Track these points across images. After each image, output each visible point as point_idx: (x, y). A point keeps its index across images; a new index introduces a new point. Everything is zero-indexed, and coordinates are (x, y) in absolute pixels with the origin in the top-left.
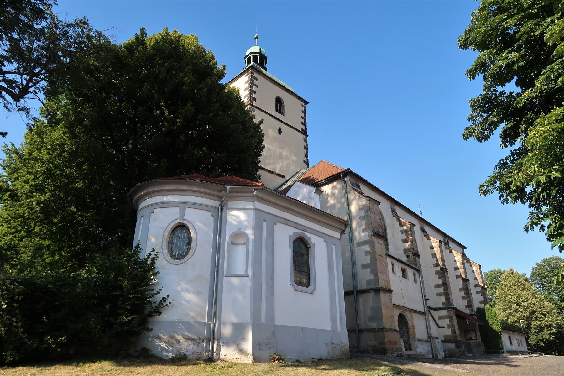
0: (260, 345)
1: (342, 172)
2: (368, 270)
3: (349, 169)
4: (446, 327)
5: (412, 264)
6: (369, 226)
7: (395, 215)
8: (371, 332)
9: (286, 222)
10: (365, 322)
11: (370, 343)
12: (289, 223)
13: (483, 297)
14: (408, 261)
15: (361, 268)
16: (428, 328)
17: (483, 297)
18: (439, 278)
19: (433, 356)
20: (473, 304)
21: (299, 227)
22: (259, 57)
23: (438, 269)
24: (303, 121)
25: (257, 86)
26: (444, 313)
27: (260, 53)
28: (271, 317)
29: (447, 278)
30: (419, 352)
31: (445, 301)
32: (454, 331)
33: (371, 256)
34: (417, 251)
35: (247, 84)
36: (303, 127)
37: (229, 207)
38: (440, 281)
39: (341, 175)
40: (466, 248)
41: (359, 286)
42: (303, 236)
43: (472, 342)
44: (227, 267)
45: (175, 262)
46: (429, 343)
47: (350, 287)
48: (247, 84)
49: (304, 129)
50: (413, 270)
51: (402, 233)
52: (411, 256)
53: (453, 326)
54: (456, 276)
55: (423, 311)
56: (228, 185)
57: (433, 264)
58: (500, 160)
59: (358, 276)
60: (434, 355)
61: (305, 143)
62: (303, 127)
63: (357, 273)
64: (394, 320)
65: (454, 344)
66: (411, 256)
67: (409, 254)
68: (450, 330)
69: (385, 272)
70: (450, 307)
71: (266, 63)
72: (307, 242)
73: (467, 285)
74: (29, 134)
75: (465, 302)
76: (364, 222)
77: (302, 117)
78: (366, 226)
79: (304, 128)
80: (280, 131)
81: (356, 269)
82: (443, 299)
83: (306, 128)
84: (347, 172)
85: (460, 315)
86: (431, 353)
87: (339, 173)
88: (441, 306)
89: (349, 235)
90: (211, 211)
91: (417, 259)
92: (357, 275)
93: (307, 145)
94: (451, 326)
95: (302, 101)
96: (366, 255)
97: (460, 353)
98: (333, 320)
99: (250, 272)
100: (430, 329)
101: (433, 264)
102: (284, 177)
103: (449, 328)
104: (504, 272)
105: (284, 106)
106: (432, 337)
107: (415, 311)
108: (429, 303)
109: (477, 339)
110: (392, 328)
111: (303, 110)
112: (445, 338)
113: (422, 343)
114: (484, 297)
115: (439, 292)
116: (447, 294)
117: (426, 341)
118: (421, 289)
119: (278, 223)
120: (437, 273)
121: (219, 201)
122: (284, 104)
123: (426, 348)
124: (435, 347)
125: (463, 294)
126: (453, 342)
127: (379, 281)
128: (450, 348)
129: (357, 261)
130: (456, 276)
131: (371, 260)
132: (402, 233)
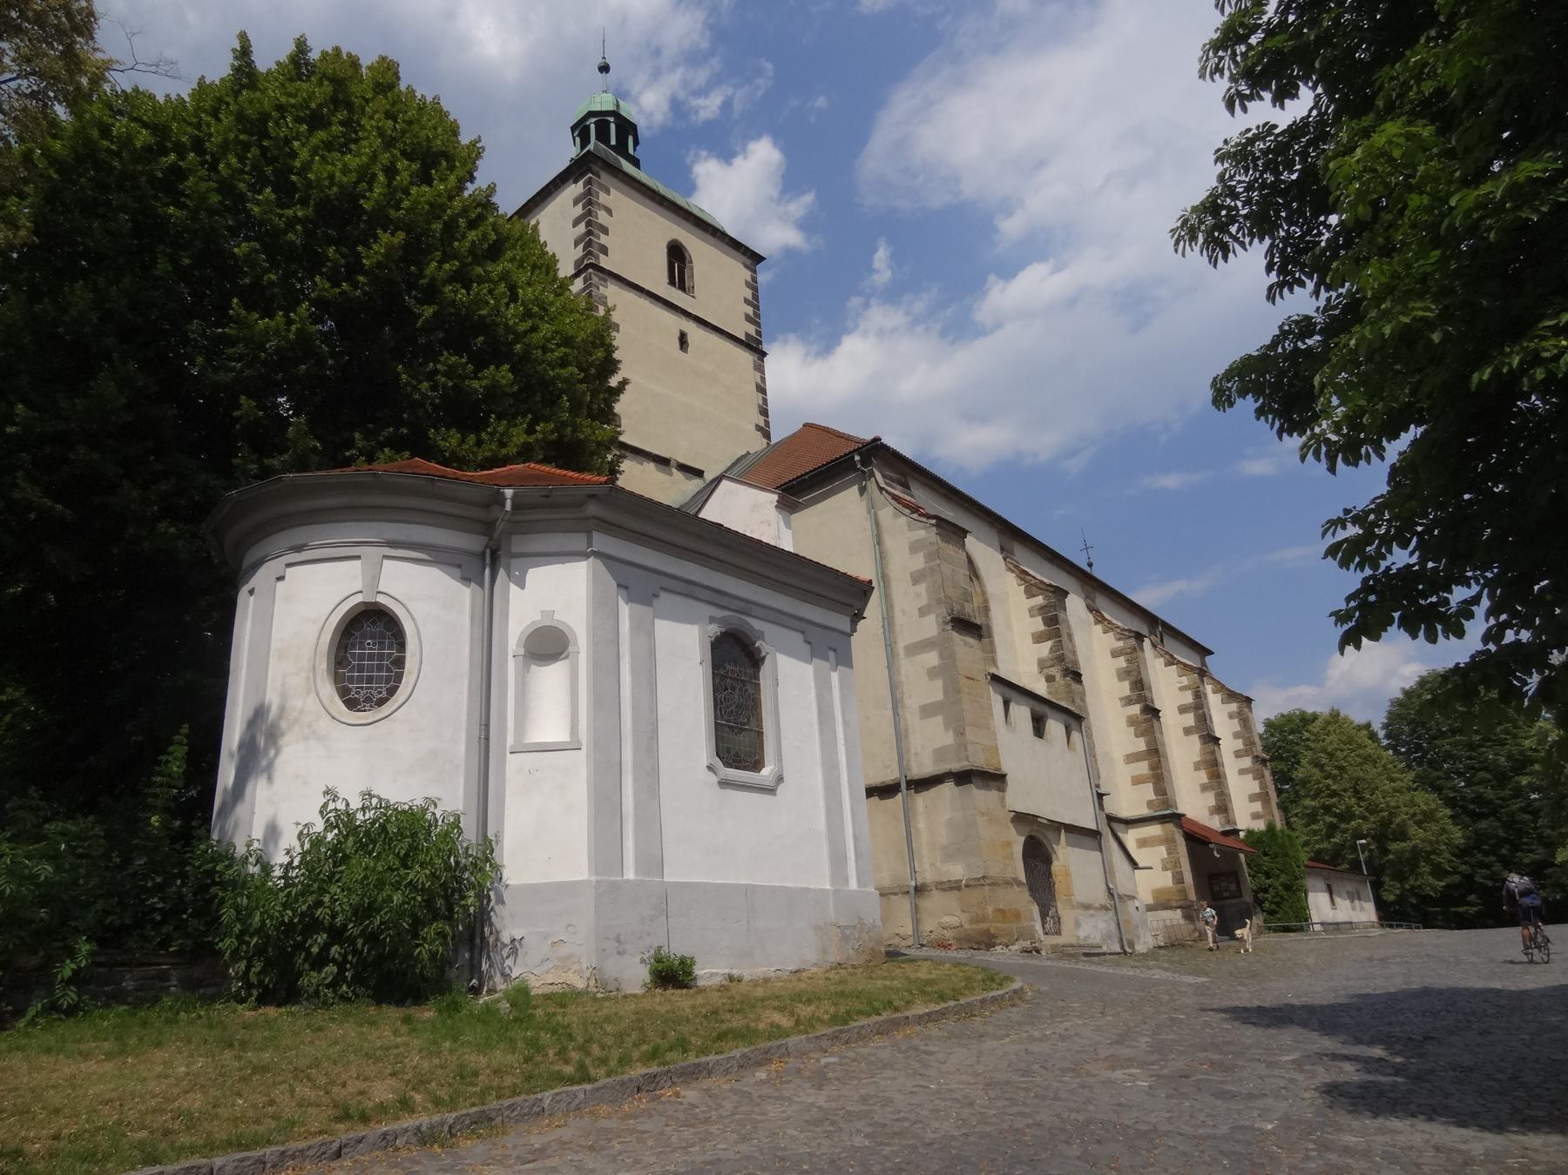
0: (618, 940)
2: (938, 721)
3: (877, 439)
4: (1158, 866)
5: (1062, 699)
7: (1011, 566)
8: (951, 889)
10: (932, 864)
11: (947, 920)
12: (697, 591)
13: (1257, 782)
14: (1049, 693)
16: (1108, 872)
17: (1257, 782)
19: (1122, 948)
20: (1231, 801)
21: (725, 601)
22: (613, 127)
24: (750, 310)
25: (609, 212)
26: (1155, 830)
27: (615, 114)
28: (653, 861)
29: (1158, 735)
30: (1082, 937)
31: (1154, 797)
32: (1179, 879)
33: (944, 681)
34: (1076, 663)
35: (580, 205)
36: (751, 329)
37: (514, 550)
38: (1141, 745)
39: (857, 458)
40: (1210, 653)
41: (913, 765)
42: (739, 627)
44: (506, 719)
45: (358, 718)
46: (1111, 914)
47: (889, 771)
48: (580, 205)
49: (753, 334)
51: (1032, 616)
52: (1058, 677)
53: (1177, 863)
55: (1093, 827)
56: (509, 486)
57: (1121, 699)
60: (1125, 942)
61: (758, 375)
62: (751, 329)
63: (906, 730)
64: (1012, 854)
65: (1179, 911)
66: (1058, 677)
67: (1053, 673)
68: (1169, 874)
69: (985, 725)
70: (1168, 812)
71: (636, 143)
73: (1213, 752)
75: (1210, 799)
76: (922, 588)
77: (746, 301)
79: (753, 333)
80: (683, 340)
81: (906, 720)
82: (1148, 792)
83: (759, 333)
84: (874, 448)
85: (1196, 840)
86: (1116, 940)
87: (850, 453)
88: (1144, 811)
89: (883, 627)
90: (459, 566)
91: (1075, 686)
92: (907, 737)
93: (763, 379)
94: (1171, 864)
95: (744, 254)
96: (931, 680)
98: (837, 860)
100: (1113, 874)
101: (1121, 699)
102: (699, 473)
103: (1165, 869)
104: (1315, 717)
105: (692, 269)
106: (1120, 897)
107: (1072, 829)
108: (1111, 806)
110: (1009, 875)
111: (749, 279)
112: (1155, 898)
113: (1091, 912)
114: (1261, 784)
115: (1137, 773)
116: (1159, 776)
117: (1104, 908)
119: (663, 595)
120: (1132, 721)
121: (484, 535)
122: (691, 262)
123: (1102, 925)
124: (1128, 922)
125: (1203, 777)
126: (1177, 908)
127: (969, 749)
128: (1168, 923)
129: (906, 696)
130: (1184, 728)
131: (946, 693)
132: (1032, 616)
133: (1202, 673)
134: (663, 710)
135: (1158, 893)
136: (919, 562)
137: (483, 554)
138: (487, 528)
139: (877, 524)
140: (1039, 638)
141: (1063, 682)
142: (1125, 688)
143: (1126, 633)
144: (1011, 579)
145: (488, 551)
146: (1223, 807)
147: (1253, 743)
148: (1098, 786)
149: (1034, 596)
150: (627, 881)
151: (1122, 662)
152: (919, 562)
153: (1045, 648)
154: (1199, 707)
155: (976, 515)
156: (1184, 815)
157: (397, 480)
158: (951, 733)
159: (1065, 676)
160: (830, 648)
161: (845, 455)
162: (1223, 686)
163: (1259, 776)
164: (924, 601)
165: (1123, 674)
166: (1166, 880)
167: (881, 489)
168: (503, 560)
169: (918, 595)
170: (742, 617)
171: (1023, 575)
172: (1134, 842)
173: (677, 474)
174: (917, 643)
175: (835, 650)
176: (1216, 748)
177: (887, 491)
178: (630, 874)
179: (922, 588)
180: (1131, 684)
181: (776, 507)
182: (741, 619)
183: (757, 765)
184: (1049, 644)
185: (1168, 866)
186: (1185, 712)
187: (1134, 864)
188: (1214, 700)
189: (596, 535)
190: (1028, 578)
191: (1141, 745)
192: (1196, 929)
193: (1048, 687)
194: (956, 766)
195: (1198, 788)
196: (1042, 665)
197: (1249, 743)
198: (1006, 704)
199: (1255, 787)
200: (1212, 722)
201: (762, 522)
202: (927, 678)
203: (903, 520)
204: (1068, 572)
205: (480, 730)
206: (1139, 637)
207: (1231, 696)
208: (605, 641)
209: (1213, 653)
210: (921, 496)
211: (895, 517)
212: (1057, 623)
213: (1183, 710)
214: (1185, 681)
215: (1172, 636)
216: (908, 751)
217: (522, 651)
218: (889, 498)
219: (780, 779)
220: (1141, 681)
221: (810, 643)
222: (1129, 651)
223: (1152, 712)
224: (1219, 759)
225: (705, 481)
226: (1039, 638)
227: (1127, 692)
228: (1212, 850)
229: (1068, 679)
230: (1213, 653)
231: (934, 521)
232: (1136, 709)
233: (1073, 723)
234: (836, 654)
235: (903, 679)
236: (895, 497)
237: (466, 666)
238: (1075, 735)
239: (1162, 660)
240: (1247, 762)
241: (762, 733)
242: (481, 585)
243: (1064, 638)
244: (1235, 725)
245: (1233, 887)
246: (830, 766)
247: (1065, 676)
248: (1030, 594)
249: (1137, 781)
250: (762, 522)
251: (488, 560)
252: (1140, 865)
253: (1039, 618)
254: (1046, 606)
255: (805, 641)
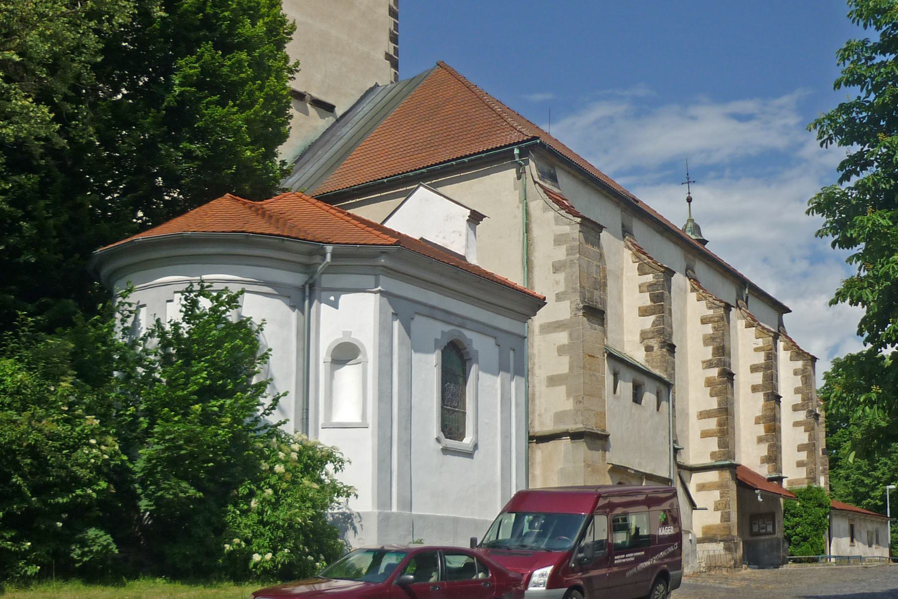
1: (519, 143)
4: (711, 507)
5: (657, 367)
6: (574, 286)
7: (629, 244)
9: (432, 312)
13: (807, 434)
14: (647, 361)
15: (545, 383)
17: (807, 434)
18: (711, 396)
23: (711, 375)
26: (712, 476)
28: (407, 503)
32: (726, 518)
38: (713, 404)
39: (516, 151)
43: (763, 540)
50: (658, 384)
51: (641, 292)
53: (727, 505)
54: (753, 386)
57: (703, 362)
58: (784, 517)
59: (537, 401)
63: (534, 395)
65: (722, 544)
67: (652, 344)
68: (719, 514)
70: (727, 462)
72: (465, 349)
73: (774, 409)
74: (738, 561)
75: (764, 450)
78: (567, 286)
81: (534, 386)
82: (713, 444)
87: (510, 145)
88: (707, 461)
90: (289, 297)
97: (733, 562)
99: (372, 419)
101: (703, 362)
103: (716, 509)
108: (682, 459)
109: (774, 533)
114: (810, 435)
118: (668, 426)
120: (709, 383)
121: (305, 273)
125: (761, 430)
126: (721, 541)
128: (711, 553)
129: (536, 367)
130: (753, 386)
131: (571, 367)
132: (641, 292)
133: (779, 333)
134: (414, 400)
135: (707, 529)
136: (561, 254)
137: (304, 286)
138: (308, 269)
139: (527, 213)
140: (644, 312)
141: (659, 353)
142: (708, 353)
143: (717, 302)
144: (627, 255)
145: (307, 286)
146: (774, 457)
147: (810, 399)
148: (675, 442)
149: (646, 274)
150: (393, 513)
151: (709, 329)
152: (561, 254)
153: (648, 322)
154: (769, 368)
155: (607, 197)
156: (739, 465)
157: (264, 239)
158: (571, 400)
159: (662, 347)
160: (511, 348)
161: (506, 146)
162: (794, 344)
163: (810, 429)
164: (561, 288)
165: (708, 340)
166: (714, 519)
167: (535, 182)
168: (317, 292)
169: (557, 283)
170: (460, 329)
171: (639, 251)
172: (695, 486)
173: (312, 110)
174: (551, 323)
175: (514, 350)
176: (777, 406)
177: (540, 185)
178: (394, 509)
179: (561, 276)
180: (714, 349)
181: (468, 221)
182: (459, 331)
183: (460, 436)
184: (652, 318)
185: (720, 507)
186: (756, 371)
187: (693, 506)
188: (783, 355)
189: (382, 278)
190: (643, 256)
191: (713, 404)
192: (733, 558)
193: (647, 356)
194: (572, 427)
195: (756, 440)
196: (644, 336)
197: (807, 399)
198: (616, 376)
199: (804, 438)
200: (777, 381)
201: (454, 232)
202: (556, 353)
203: (551, 214)
204: (675, 243)
205: (303, 413)
206: (728, 307)
207: (798, 353)
208: (385, 354)
209: (790, 311)
210: (567, 184)
211: (545, 210)
212: (662, 300)
213: (754, 369)
214: (760, 343)
215: (756, 297)
216: (533, 412)
217: (330, 359)
218: (541, 191)
219: (476, 446)
220: (723, 348)
221: (499, 346)
222: (716, 319)
223: (728, 376)
224: (778, 416)
225: (335, 116)
226: (644, 312)
227: (709, 356)
228: (757, 495)
229: (664, 350)
230: (790, 311)
231: (579, 220)
232: (714, 372)
233: (664, 390)
234: (515, 353)
235: (536, 351)
236: (546, 191)
237: (294, 368)
238: (664, 404)
239: (744, 321)
240: (802, 416)
241: (465, 413)
242: (302, 311)
243: (666, 314)
244: (798, 382)
245: (770, 529)
246: (506, 436)
247: (662, 347)
248: (642, 272)
249: (705, 434)
250: (454, 232)
251: (307, 293)
252: (698, 507)
253: (647, 295)
254: (655, 284)
255: (496, 344)
